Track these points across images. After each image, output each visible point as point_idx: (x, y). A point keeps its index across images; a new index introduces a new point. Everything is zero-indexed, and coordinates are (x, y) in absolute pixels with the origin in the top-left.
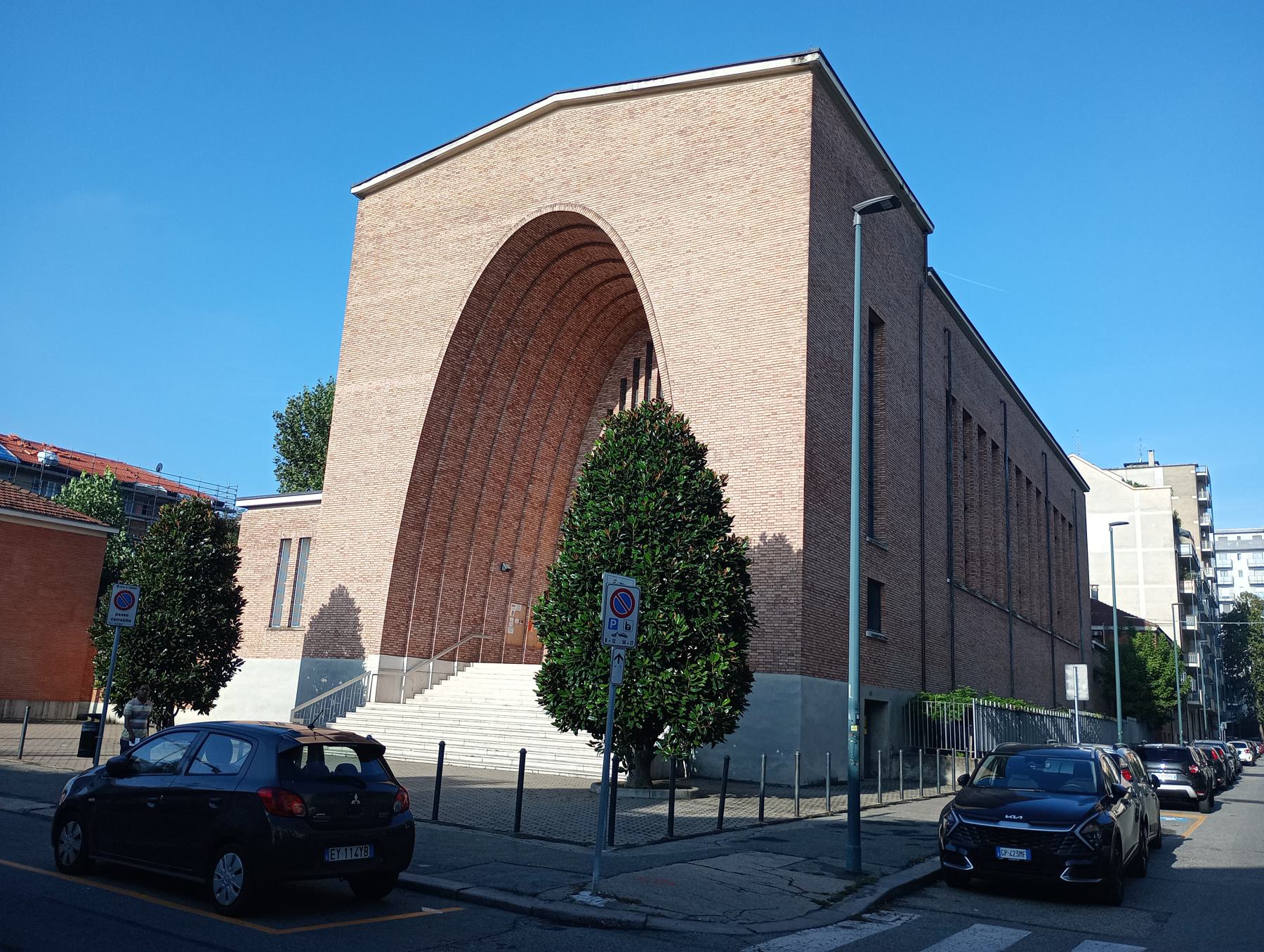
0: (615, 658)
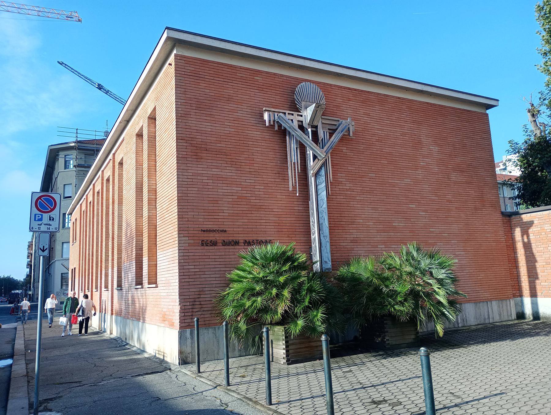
0: (47, 249)
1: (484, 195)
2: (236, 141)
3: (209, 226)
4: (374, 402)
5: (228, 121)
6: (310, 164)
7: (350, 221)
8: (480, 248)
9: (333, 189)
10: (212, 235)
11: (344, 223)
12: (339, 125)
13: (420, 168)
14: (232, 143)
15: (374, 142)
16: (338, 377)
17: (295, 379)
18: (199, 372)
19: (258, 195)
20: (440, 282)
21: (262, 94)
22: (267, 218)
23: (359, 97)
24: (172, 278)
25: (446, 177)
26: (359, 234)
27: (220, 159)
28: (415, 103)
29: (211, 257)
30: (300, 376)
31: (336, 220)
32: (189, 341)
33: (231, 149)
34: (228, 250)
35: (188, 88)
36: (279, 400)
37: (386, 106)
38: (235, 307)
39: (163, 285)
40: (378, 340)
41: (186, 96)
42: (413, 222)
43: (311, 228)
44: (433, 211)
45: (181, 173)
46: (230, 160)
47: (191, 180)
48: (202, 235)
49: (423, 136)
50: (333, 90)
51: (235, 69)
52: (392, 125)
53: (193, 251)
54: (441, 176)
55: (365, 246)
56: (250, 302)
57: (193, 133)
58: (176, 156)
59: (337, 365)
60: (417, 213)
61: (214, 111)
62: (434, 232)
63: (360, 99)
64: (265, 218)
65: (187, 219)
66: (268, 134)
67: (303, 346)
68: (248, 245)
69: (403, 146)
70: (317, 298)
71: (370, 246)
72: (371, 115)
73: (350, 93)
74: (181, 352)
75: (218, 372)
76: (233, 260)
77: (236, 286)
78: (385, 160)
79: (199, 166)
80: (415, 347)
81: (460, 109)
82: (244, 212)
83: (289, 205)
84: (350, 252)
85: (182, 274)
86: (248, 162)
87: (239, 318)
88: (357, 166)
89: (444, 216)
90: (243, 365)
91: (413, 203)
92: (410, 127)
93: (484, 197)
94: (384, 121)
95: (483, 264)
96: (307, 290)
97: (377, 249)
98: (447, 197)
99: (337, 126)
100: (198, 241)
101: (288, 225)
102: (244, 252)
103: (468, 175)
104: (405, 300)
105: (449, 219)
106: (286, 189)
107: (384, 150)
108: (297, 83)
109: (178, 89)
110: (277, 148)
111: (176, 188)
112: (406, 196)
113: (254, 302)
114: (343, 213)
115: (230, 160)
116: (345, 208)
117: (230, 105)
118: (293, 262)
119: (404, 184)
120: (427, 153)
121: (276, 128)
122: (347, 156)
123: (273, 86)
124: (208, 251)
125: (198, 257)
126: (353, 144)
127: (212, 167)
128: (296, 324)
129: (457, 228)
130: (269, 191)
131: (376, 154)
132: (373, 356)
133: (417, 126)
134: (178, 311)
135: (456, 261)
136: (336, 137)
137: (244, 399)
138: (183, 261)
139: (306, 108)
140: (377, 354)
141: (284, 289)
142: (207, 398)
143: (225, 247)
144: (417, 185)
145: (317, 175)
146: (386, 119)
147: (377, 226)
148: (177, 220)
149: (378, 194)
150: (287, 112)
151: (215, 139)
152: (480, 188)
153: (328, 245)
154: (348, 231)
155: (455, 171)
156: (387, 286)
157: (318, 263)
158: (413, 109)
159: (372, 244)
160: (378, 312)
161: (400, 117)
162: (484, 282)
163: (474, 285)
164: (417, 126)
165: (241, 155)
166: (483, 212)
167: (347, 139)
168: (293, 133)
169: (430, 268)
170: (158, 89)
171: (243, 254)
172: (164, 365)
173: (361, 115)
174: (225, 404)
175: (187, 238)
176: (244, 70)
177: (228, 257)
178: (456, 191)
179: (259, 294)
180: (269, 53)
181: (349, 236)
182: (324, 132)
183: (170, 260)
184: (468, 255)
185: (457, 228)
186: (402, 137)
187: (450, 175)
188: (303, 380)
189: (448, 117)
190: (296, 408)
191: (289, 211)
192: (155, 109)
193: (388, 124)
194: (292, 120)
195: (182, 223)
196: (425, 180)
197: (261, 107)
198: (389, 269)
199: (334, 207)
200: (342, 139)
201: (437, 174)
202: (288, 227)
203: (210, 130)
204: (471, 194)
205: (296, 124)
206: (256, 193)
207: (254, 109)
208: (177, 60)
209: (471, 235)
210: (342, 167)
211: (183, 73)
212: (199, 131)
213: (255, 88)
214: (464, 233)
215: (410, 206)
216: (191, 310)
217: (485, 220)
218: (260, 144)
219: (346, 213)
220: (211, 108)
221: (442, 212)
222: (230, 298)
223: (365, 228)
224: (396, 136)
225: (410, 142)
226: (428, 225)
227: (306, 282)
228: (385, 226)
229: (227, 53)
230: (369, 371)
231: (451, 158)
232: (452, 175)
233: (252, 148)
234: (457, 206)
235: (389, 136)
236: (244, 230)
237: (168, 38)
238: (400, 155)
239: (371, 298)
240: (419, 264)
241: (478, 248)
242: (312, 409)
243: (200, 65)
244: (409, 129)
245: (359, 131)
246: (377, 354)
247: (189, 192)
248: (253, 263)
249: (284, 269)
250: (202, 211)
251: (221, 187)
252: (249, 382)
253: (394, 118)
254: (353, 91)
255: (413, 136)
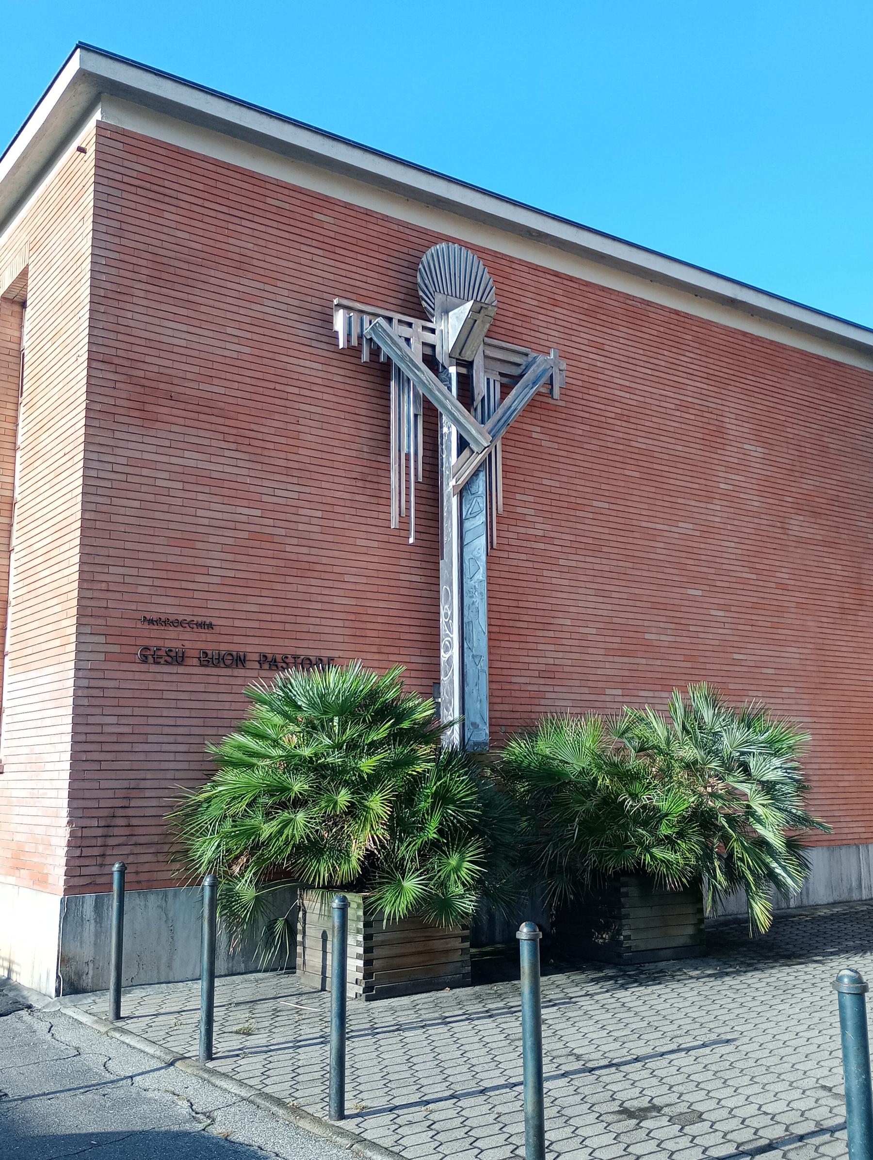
1: (863, 576)
2: (254, 382)
3: (167, 608)
4: (626, 1113)
5: (236, 325)
6: (449, 463)
7: (539, 619)
8: (847, 710)
9: (502, 534)
10: (173, 635)
11: (525, 625)
12: (528, 367)
13: (717, 496)
14: (242, 387)
15: (609, 421)
16: (511, 1037)
17: (394, 1040)
18: (118, 1017)
19: (305, 535)
20: (769, 788)
21: (332, 263)
22: (325, 599)
23: (581, 298)
24: (49, 748)
25: (779, 524)
26: (560, 655)
27: (207, 426)
28: (714, 329)
29: (166, 695)
30: (406, 1034)
31: (504, 616)
32: (90, 928)
33: (240, 401)
34: (213, 680)
35: (130, 220)
36: (364, 1104)
37: (644, 329)
38: (228, 835)
39: (22, 767)
40: (602, 938)
41: (124, 242)
42: (695, 635)
43: (442, 633)
44: (744, 610)
45: (94, 456)
46: (234, 431)
47: (174, 444)
48: (146, 633)
49: (728, 415)
50: (517, 273)
51: (262, 184)
52: (656, 379)
53: (117, 675)
54: (765, 522)
55: (574, 690)
56: (274, 823)
57: (136, 349)
58: (84, 406)
59: (501, 1004)
60: (706, 612)
61: (198, 292)
62: (743, 663)
63: (581, 304)
64: (320, 598)
65: (104, 586)
66: (342, 372)
67: (410, 948)
68: (270, 669)
69: (679, 436)
70: (459, 821)
71: (586, 690)
72: (606, 348)
73: (559, 286)
74: (63, 960)
75: (172, 1020)
76: (227, 706)
77: (231, 778)
78: (633, 468)
79: (147, 440)
80: (695, 958)
81: (818, 357)
82: (265, 577)
83: (387, 568)
84: (537, 701)
85: (82, 738)
86: (283, 440)
87: (236, 869)
88: (565, 479)
89: (769, 624)
90: (242, 999)
91: (697, 586)
92: (699, 390)
93: (864, 582)
94: (638, 369)
95: (853, 749)
96: (435, 795)
97: (602, 698)
98: (778, 575)
99: (523, 367)
100: (132, 650)
101: (380, 619)
102: (263, 686)
103: (829, 523)
104: (681, 835)
105: (780, 631)
106: (379, 523)
107: (633, 444)
108: (426, 243)
109: (100, 220)
110: (363, 412)
111: (80, 498)
112: (680, 566)
113: (287, 823)
114: (524, 598)
115: (234, 431)
116: (530, 584)
117: (243, 281)
118: (400, 718)
119: (677, 536)
120: (736, 461)
121: (365, 357)
122: (541, 449)
123: (360, 243)
124: (159, 677)
125: (129, 694)
126: (559, 422)
127: (182, 445)
128: (400, 890)
129: (797, 656)
130: (337, 524)
131: (613, 452)
132: (592, 980)
133: (716, 389)
134: (64, 842)
135: (809, 738)
136: (519, 397)
137: (259, 1101)
138: (85, 702)
139: (446, 312)
140: (601, 974)
141: (372, 792)
142: (150, 1095)
143: (208, 670)
144: (709, 541)
145: (462, 492)
146: (642, 364)
147: (608, 639)
148: (76, 585)
149: (612, 556)
150: (397, 316)
151: (196, 369)
152: (854, 559)
153: (484, 679)
154: (534, 646)
155: (799, 512)
156: (634, 796)
157: (457, 727)
158: (708, 343)
159: (590, 684)
160: (611, 864)
161: (678, 362)
162: (854, 795)
163: (828, 802)
164: (716, 389)
165: (264, 421)
166: (860, 618)
167: (544, 405)
168: (407, 373)
169: (743, 754)
170: (39, 219)
171: (260, 691)
172: (11, 994)
173: (583, 347)
174: (204, 1114)
175: (102, 639)
176: (286, 192)
177: (213, 697)
178: (799, 561)
179: (299, 803)
180: (358, 153)
181: (535, 660)
182: (488, 379)
183: (47, 696)
184: (819, 726)
185: (797, 656)
186: (678, 413)
187: (787, 521)
188: (417, 1045)
189: (791, 373)
190: (416, 1128)
191: (386, 582)
192: (24, 274)
193: (646, 377)
194: (408, 340)
195: (89, 594)
196: (729, 527)
197: (326, 296)
198: (642, 749)
199: (501, 581)
200: (532, 405)
201: (756, 515)
202: (380, 627)
203: (183, 343)
204: (833, 572)
205: (416, 352)
206: (301, 527)
207: (309, 299)
208: (102, 140)
209: (829, 675)
210: (528, 479)
211: (118, 177)
212: (153, 344)
213: (315, 243)
214: (811, 668)
215: (690, 592)
216: (100, 842)
217: (861, 640)
218: (319, 395)
219: (531, 598)
220: (190, 282)
221: (764, 612)
222: (215, 811)
223: (576, 643)
224: (664, 410)
225: (698, 429)
226: (731, 644)
227: (432, 776)
228: (625, 640)
229: (243, 138)
230: (592, 1022)
231: (792, 478)
232: (792, 522)
233: (296, 406)
234: (800, 600)
235: (648, 406)
236: (263, 625)
237: (83, 75)
238: (671, 458)
239: (590, 827)
240: (715, 742)
241: (843, 709)
242: (460, 1133)
243: (167, 161)
244: (696, 395)
245: (574, 388)
246: (601, 974)
247: (114, 510)
248: (285, 715)
249: (374, 736)
250: (150, 565)
251: (206, 505)
252: (267, 1050)
253: (663, 363)
254: (565, 282)
255: (705, 414)
